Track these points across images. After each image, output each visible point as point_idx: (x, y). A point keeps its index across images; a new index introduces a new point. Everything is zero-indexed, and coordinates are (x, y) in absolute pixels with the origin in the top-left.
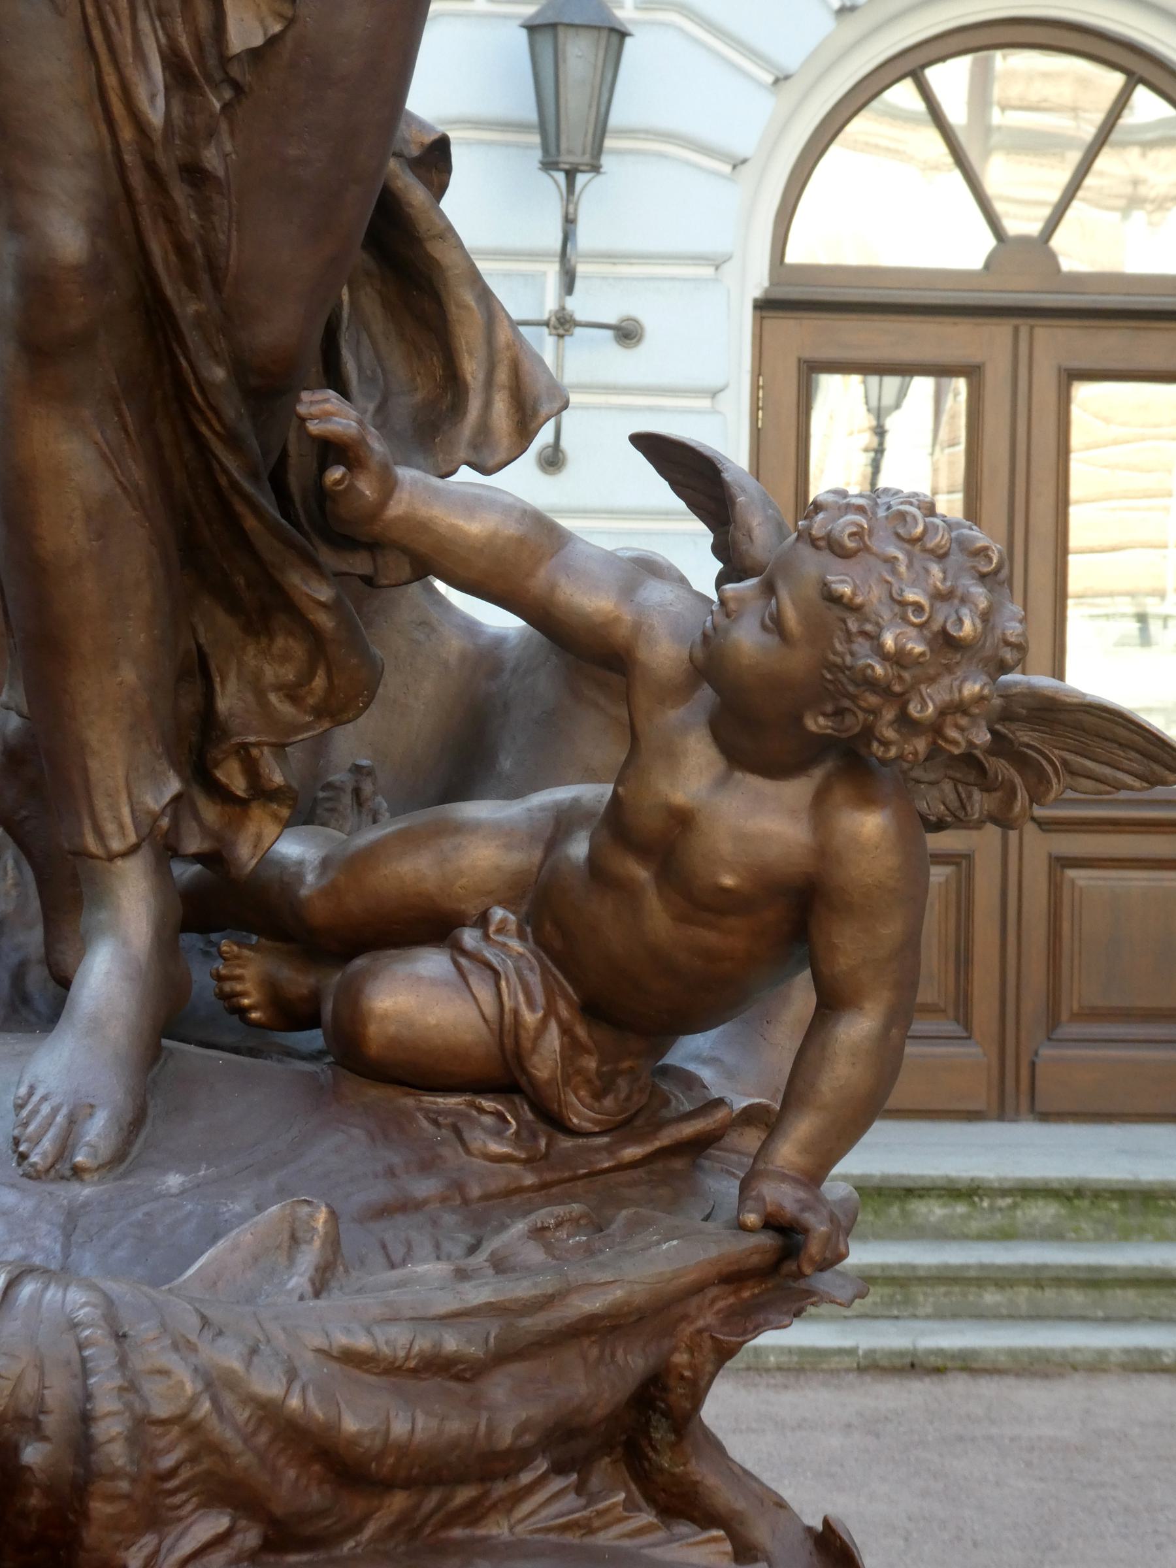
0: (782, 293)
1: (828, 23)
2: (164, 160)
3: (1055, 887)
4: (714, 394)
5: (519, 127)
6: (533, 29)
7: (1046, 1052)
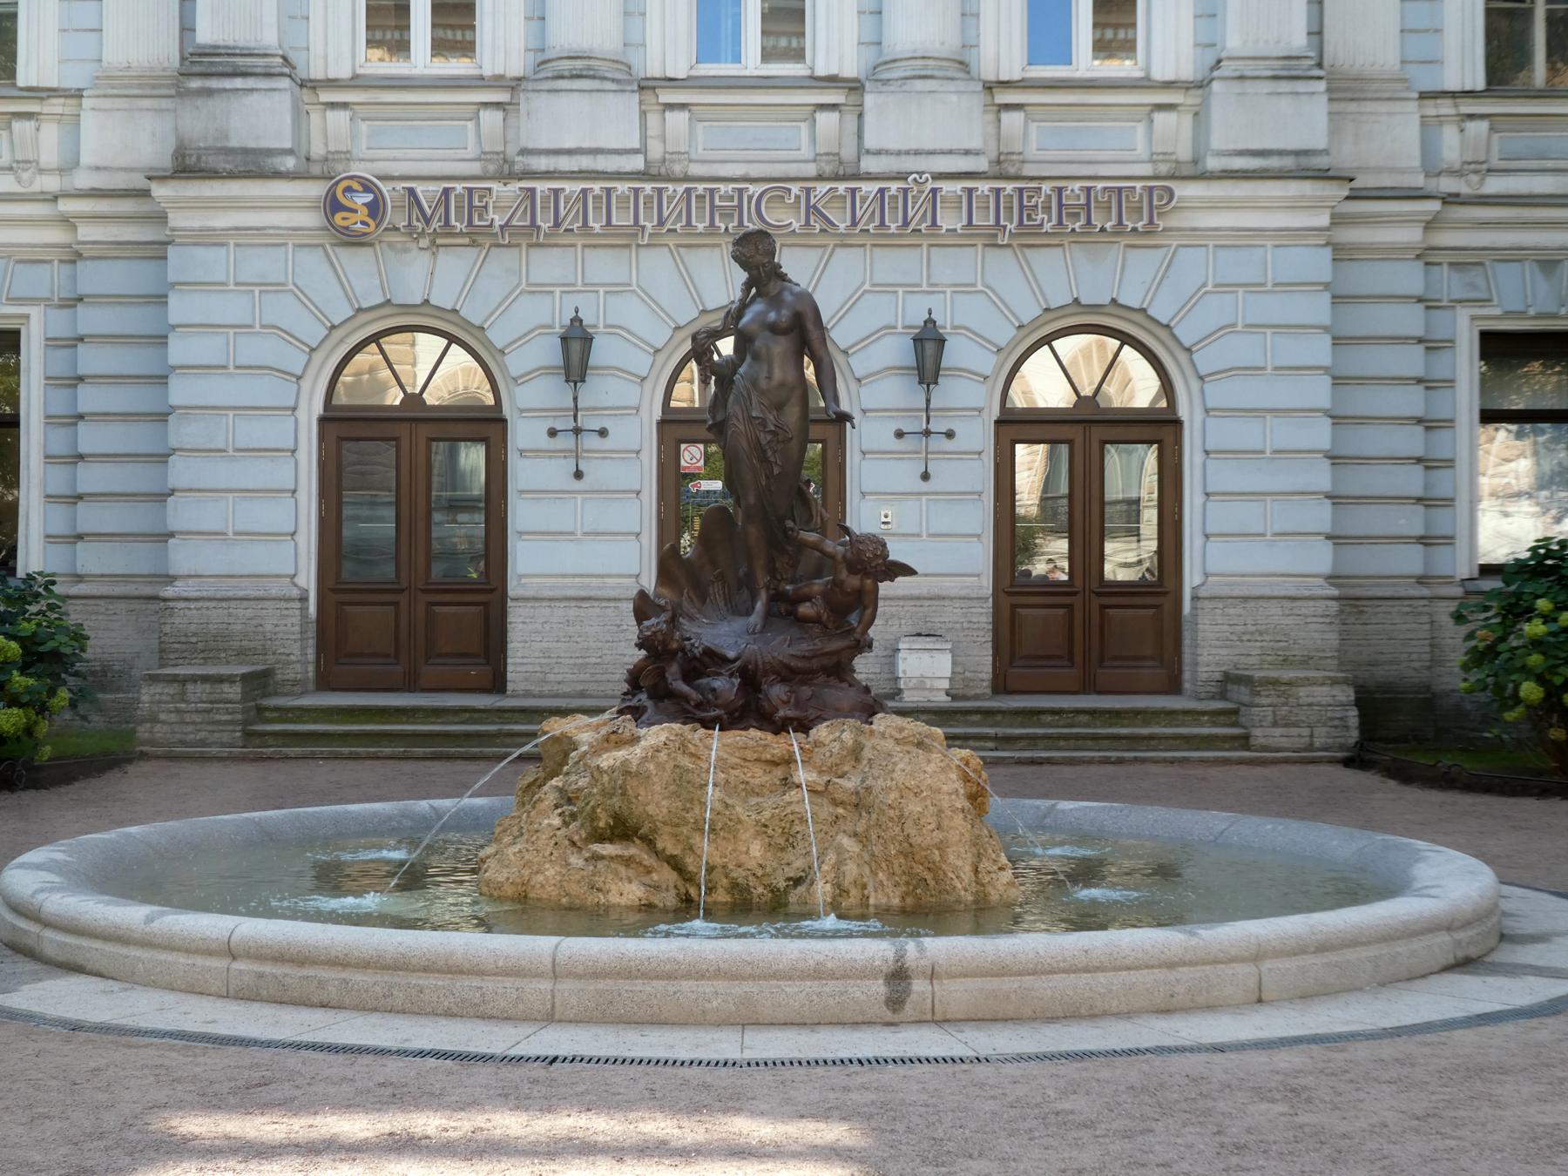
0: (1005, 418)
1: (1014, 332)
2: (592, 988)
3: (1102, 616)
4: (980, 453)
5: (913, 369)
6: (915, 340)
7: (1100, 671)
